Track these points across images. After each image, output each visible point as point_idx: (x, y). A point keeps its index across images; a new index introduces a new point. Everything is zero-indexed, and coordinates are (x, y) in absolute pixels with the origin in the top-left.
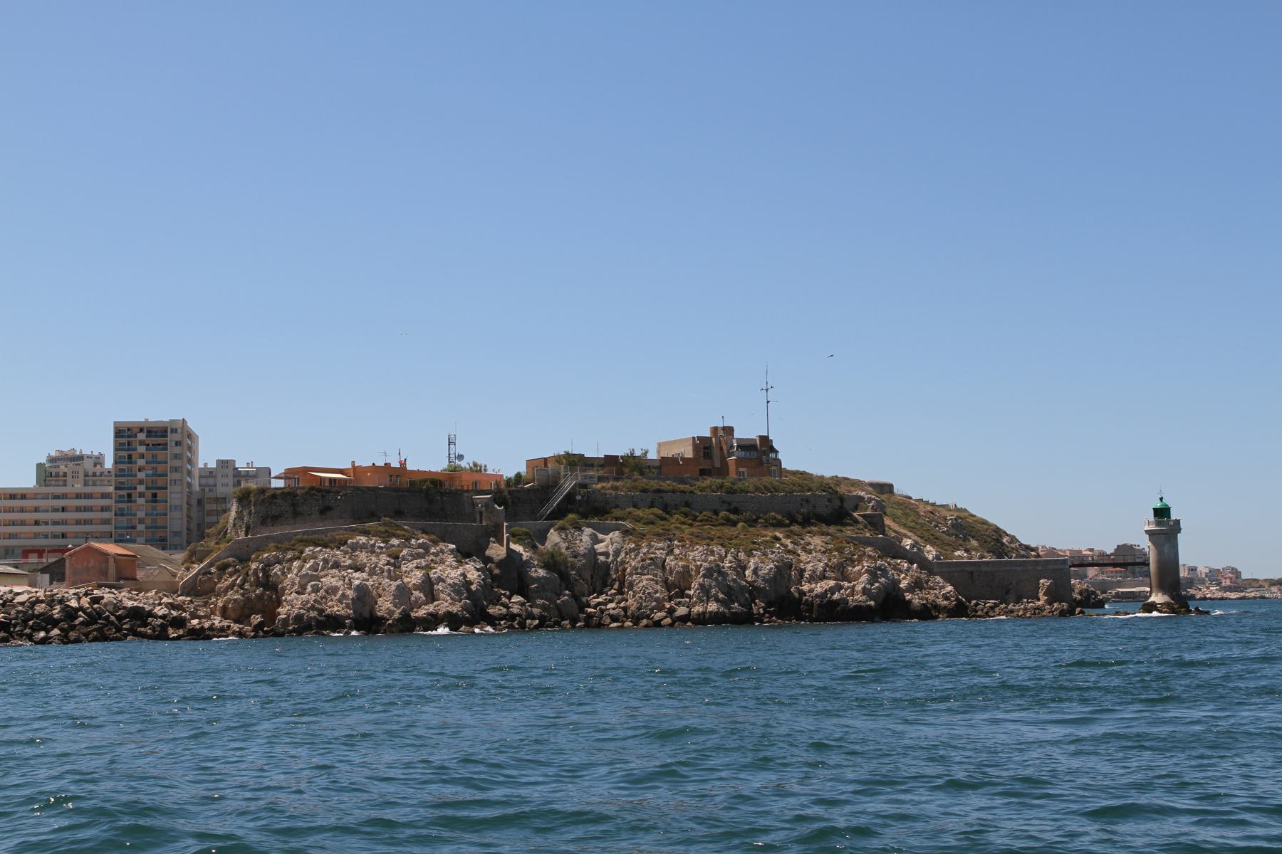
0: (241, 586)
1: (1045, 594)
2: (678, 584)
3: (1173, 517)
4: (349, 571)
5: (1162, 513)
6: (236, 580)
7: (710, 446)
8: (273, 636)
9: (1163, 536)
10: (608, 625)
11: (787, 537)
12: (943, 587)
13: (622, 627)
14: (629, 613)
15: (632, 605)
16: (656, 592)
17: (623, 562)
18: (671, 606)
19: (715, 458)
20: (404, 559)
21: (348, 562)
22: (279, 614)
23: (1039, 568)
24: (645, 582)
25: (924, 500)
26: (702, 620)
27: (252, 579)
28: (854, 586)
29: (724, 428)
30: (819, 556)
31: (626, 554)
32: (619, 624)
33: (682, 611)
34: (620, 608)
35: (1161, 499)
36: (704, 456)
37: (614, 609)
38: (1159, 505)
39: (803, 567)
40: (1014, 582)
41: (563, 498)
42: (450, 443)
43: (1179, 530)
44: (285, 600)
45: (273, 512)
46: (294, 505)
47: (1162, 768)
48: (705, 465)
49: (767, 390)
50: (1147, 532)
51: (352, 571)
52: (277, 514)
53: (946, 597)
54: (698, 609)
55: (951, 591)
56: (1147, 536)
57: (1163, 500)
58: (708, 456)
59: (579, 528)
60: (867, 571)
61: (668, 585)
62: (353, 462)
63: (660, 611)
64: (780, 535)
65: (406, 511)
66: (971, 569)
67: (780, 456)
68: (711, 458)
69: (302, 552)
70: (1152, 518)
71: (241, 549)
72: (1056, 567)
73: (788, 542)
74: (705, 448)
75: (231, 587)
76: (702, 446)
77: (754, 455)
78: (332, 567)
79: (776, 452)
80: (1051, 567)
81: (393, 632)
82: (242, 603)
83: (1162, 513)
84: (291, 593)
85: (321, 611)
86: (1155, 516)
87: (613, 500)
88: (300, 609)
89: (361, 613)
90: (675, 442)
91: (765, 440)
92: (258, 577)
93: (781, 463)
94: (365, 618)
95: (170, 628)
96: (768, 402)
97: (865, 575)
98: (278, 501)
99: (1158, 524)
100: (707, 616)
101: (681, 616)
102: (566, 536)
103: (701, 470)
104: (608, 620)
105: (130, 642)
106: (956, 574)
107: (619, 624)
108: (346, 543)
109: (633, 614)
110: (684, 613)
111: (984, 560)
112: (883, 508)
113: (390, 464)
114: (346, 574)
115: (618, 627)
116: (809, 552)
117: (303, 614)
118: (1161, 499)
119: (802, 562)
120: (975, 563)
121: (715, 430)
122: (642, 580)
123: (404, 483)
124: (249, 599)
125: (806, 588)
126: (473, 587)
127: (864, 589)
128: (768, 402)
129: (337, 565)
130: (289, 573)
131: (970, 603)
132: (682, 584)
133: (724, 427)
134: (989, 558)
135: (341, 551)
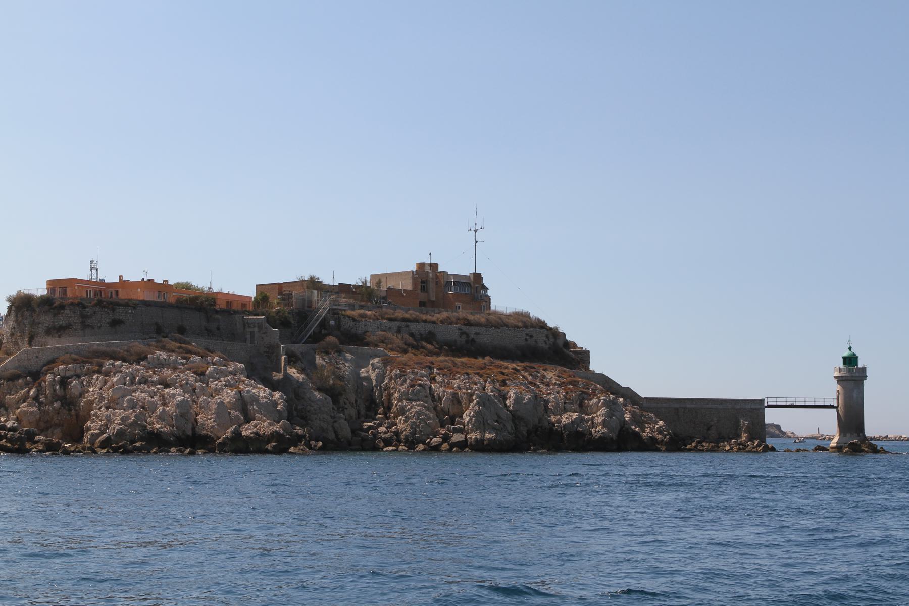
0: (36, 398)
1: (745, 432)
2: (447, 411)
3: (860, 365)
4: (158, 386)
5: (850, 361)
6: (29, 392)
7: (427, 281)
8: (122, 453)
9: (854, 382)
10: (382, 449)
12: (656, 423)
13: (397, 450)
14: (402, 437)
15: (405, 430)
16: (429, 418)
17: (387, 388)
18: (446, 432)
20: (211, 376)
21: (155, 378)
22: (89, 429)
24: (417, 408)
26: (481, 447)
27: (48, 392)
28: (593, 418)
29: (431, 265)
30: (557, 389)
31: (391, 379)
32: (394, 448)
33: (457, 438)
34: (391, 432)
35: (850, 349)
36: (101, 293)
37: (385, 433)
38: (846, 353)
39: (546, 399)
40: (715, 419)
41: (318, 325)
42: (92, 268)
43: (865, 377)
44: (94, 415)
45: (61, 323)
46: (84, 317)
48: (422, 297)
49: (476, 231)
50: (835, 377)
51: (161, 386)
52: (64, 325)
53: (660, 431)
54: (474, 436)
55: (663, 426)
57: (852, 350)
58: (424, 290)
59: (340, 352)
60: (603, 405)
61: (440, 413)
62: (121, 277)
63: (435, 437)
65: (188, 328)
66: (677, 405)
67: (490, 293)
68: (427, 292)
69: (101, 365)
70: (842, 365)
71: (30, 359)
72: (753, 406)
74: (422, 282)
75: (24, 399)
76: (420, 280)
77: (468, 291)
78: (140, 383)
79: (486, 289)
81: (225, 452)
82: (38, 416)
83: (850, 361)
84: (100, 408)
85: (144, 428)
86: (845, 363)
87: (363, 326)
88: (120, 424)
89: (184, 431)
90: (396, 274)
91: (478, 277)
92: (55, 390)
93: (490, 299)
94: (188, 436)
95: (485, 444)
96: (476, 242)
97: (603, 408)
98: (66, 311)
99: (849, 371)
100: (486, 443)
101: (458, 442)
102: (330, 359)
103: (420, 302)
104: (382, 445)
105: (47, 456)
107: (394, 448)
108: (146, 358)
109: (406, 438)
110: (461, 440)
113: (153, 280)
114: (156, 390)
115: (393, 450)
117: (125, 431)
118: (850, 349)
119: (544, 394)
122: (413, 405)
123: (171, 299)
124: (46, 412)
125: (553, 418)
126: (511, 408)
127: (604, 421)
128: (476, 242)
129: (144, 381)
130: (89, 386)
131: (368, 433)
132: (451, 410)
133: (431, 263)
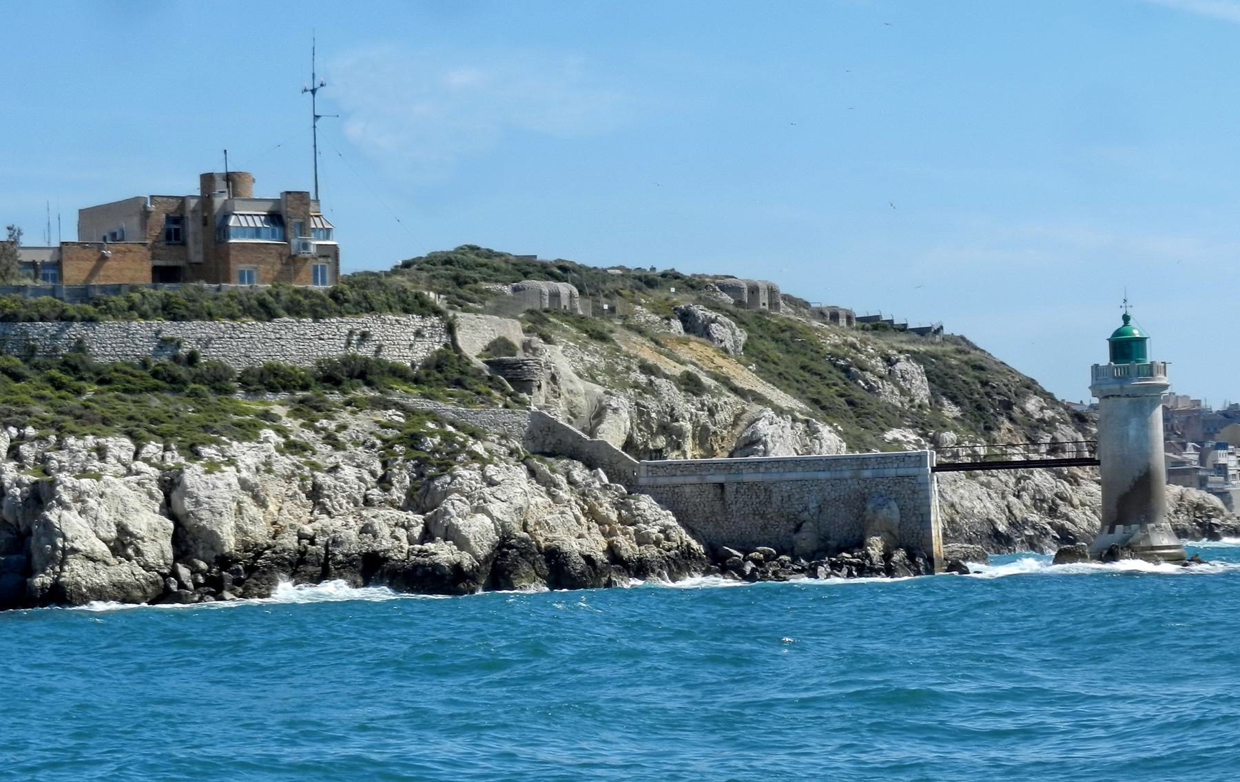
9: (1125, 401)
11: (296, 413)
19: (190, 240)
23: (867, 474)
25: (21, 237)
40: (812, 505)
47: (1159, 764)
49: (313, 91)
56: (190, 187)
58: (177, 238)
64: (278, 410)
66: (720, 478)
73: (292, 424)
80: (891, 472)
96: (316, 117)
106: (688, 490)
111: (752, 457)
112: (86, 295)
116: (337, 446)
120: (726, 467)
121: (207, 180)
128: (316, 117)
134: (831, 442)
135: (317, 431)
